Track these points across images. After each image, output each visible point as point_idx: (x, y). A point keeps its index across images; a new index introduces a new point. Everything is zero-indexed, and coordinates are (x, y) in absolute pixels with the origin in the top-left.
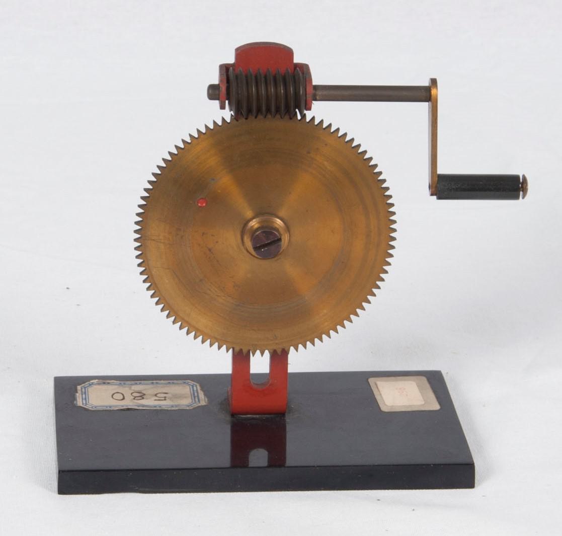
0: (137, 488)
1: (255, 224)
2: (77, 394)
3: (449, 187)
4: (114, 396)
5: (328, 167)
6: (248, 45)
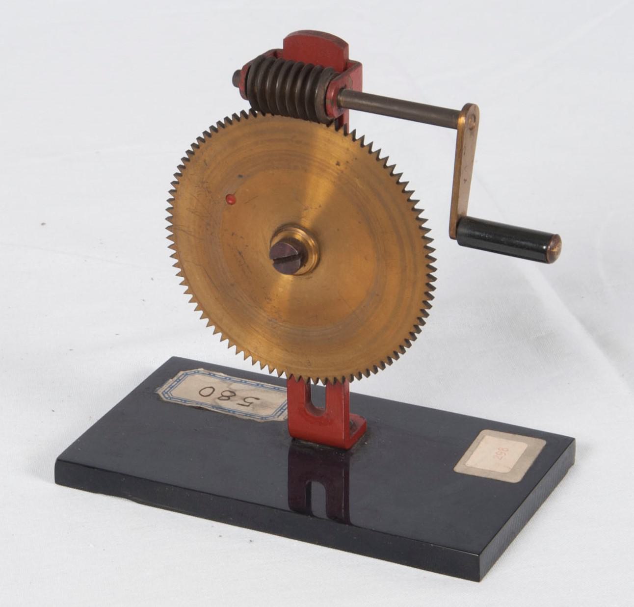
0: (130, 496)
1: (300, 235)
2: (171, 380)
3: (473, 233)
4: (201, 393)
5: (359, 185)
6: (300, 32)
